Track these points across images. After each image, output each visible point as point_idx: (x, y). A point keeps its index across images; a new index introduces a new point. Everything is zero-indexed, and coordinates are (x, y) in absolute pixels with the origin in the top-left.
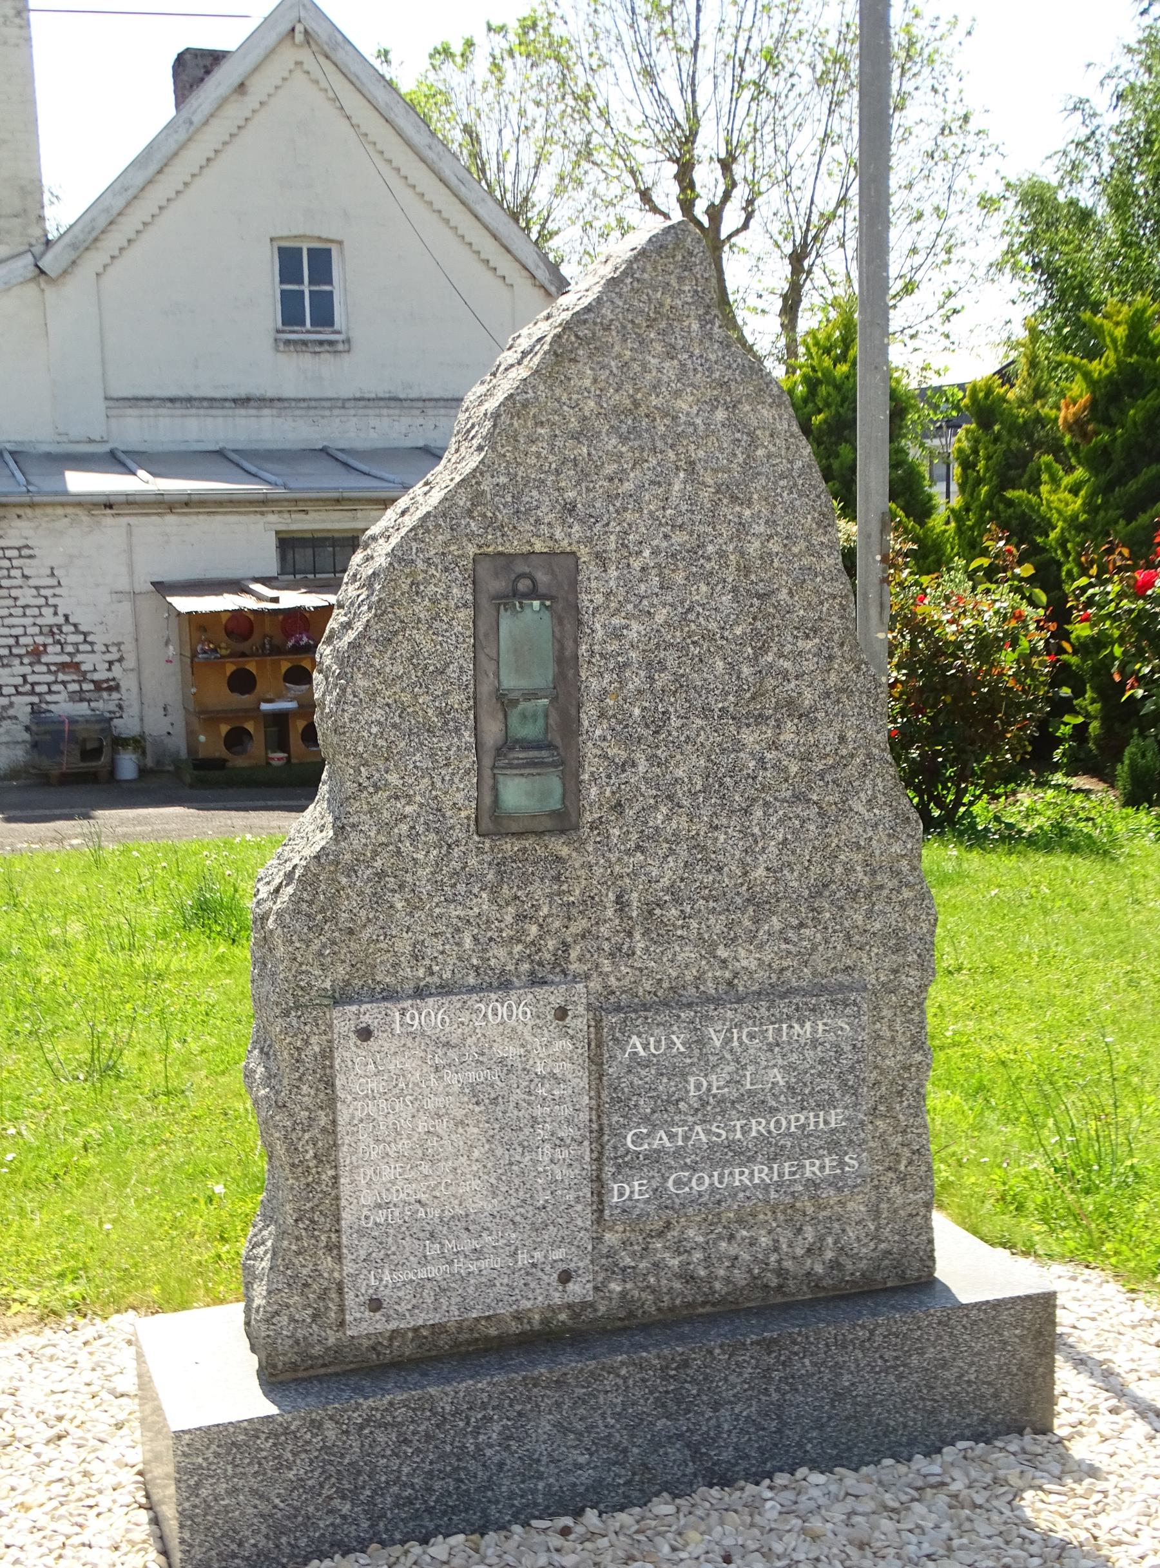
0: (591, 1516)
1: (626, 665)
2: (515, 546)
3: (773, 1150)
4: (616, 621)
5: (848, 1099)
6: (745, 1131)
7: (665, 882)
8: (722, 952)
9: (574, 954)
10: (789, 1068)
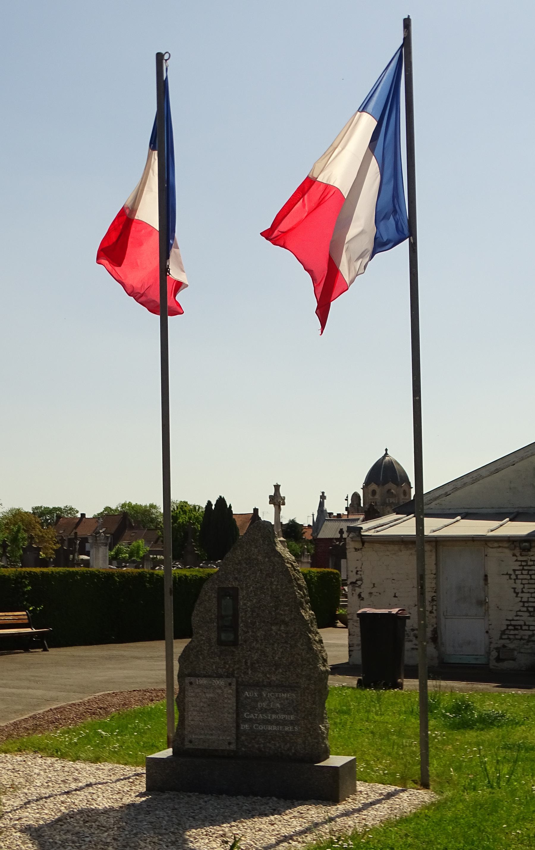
0: (224, 795)
1: (247, 611)
2: (225, 586)
3: (277, 723)
4: (245, 602)
5: (295, 713)
6: (271, 717)
7: (255, 658)
8: (268, 676)
9: (236, 672)
10: (281, 704)
